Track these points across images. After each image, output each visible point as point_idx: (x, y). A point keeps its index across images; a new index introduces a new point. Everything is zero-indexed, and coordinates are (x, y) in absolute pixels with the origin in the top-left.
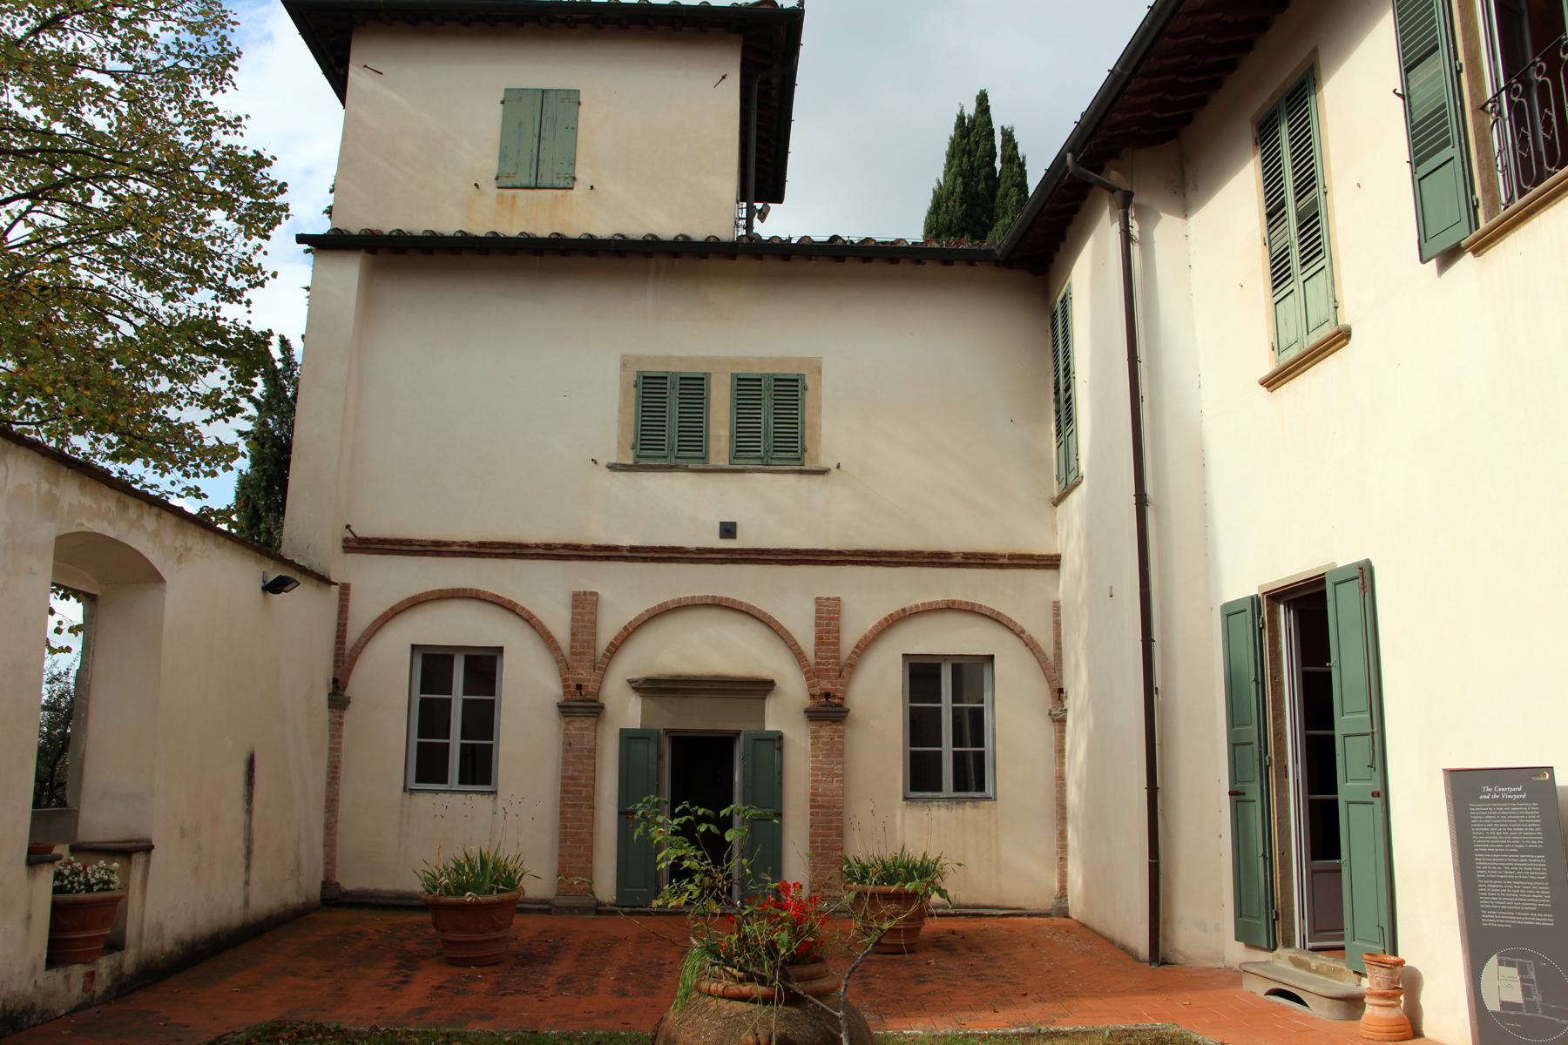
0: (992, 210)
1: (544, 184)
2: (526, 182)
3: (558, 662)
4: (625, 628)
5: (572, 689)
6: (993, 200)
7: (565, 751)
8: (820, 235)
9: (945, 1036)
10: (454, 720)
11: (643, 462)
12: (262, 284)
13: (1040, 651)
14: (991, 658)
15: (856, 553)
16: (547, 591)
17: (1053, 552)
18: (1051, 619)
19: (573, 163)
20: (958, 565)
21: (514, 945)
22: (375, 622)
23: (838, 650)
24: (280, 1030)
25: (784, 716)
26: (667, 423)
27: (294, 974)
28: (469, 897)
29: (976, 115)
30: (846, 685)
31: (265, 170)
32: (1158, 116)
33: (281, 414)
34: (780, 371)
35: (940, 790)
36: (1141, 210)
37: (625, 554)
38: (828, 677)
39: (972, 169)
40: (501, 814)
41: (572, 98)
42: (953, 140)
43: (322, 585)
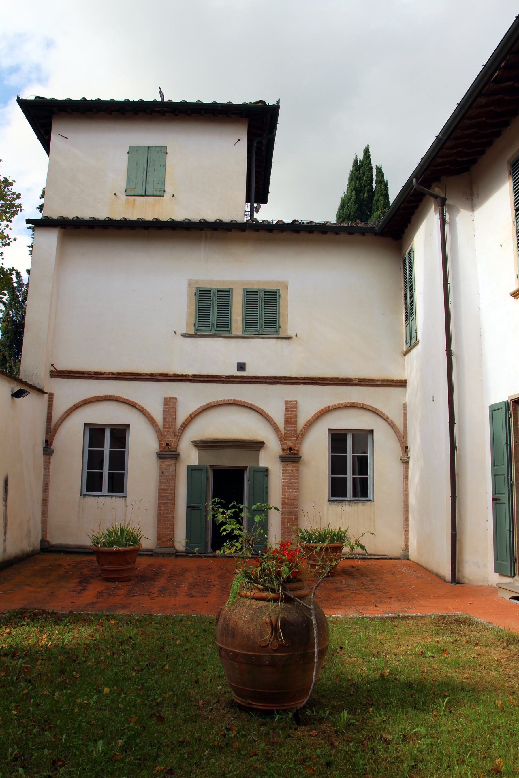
0: (371, 207)
1: (149, 194)
2: (140, 193)
3: (157, 432)
4: (190, 415)
5: (164, 446)
6: (372, 203)
7: (160, 476)
8: (288, 219)
9: (353, 618)
10: (106, 460)
11: (199, 333)
12: (9, 244)
13: (396, 428)
14: (372, 431)
15: (305, 378)
16: (151, 396)
17: (403, 379)
18: (402, 412)
19: (163, 183)
20: (356, 385)
21: (136, 572)
22: (66, 412)
24: (25, 612)
25: (269, 459)
26: (211, 312)
27: (30, 585)
28: (115, 548)
29: (363, 160)
30: (300, 444)
31: (10, 188)
32: (460, 160)
33: (16, 309)
35: (346, 496)
36: (450, 207)
38: (291, 440)
39: (361, 187)
40: (129, 508)
41: (163, 151)
42: (352, 172)
43: (40, 394)
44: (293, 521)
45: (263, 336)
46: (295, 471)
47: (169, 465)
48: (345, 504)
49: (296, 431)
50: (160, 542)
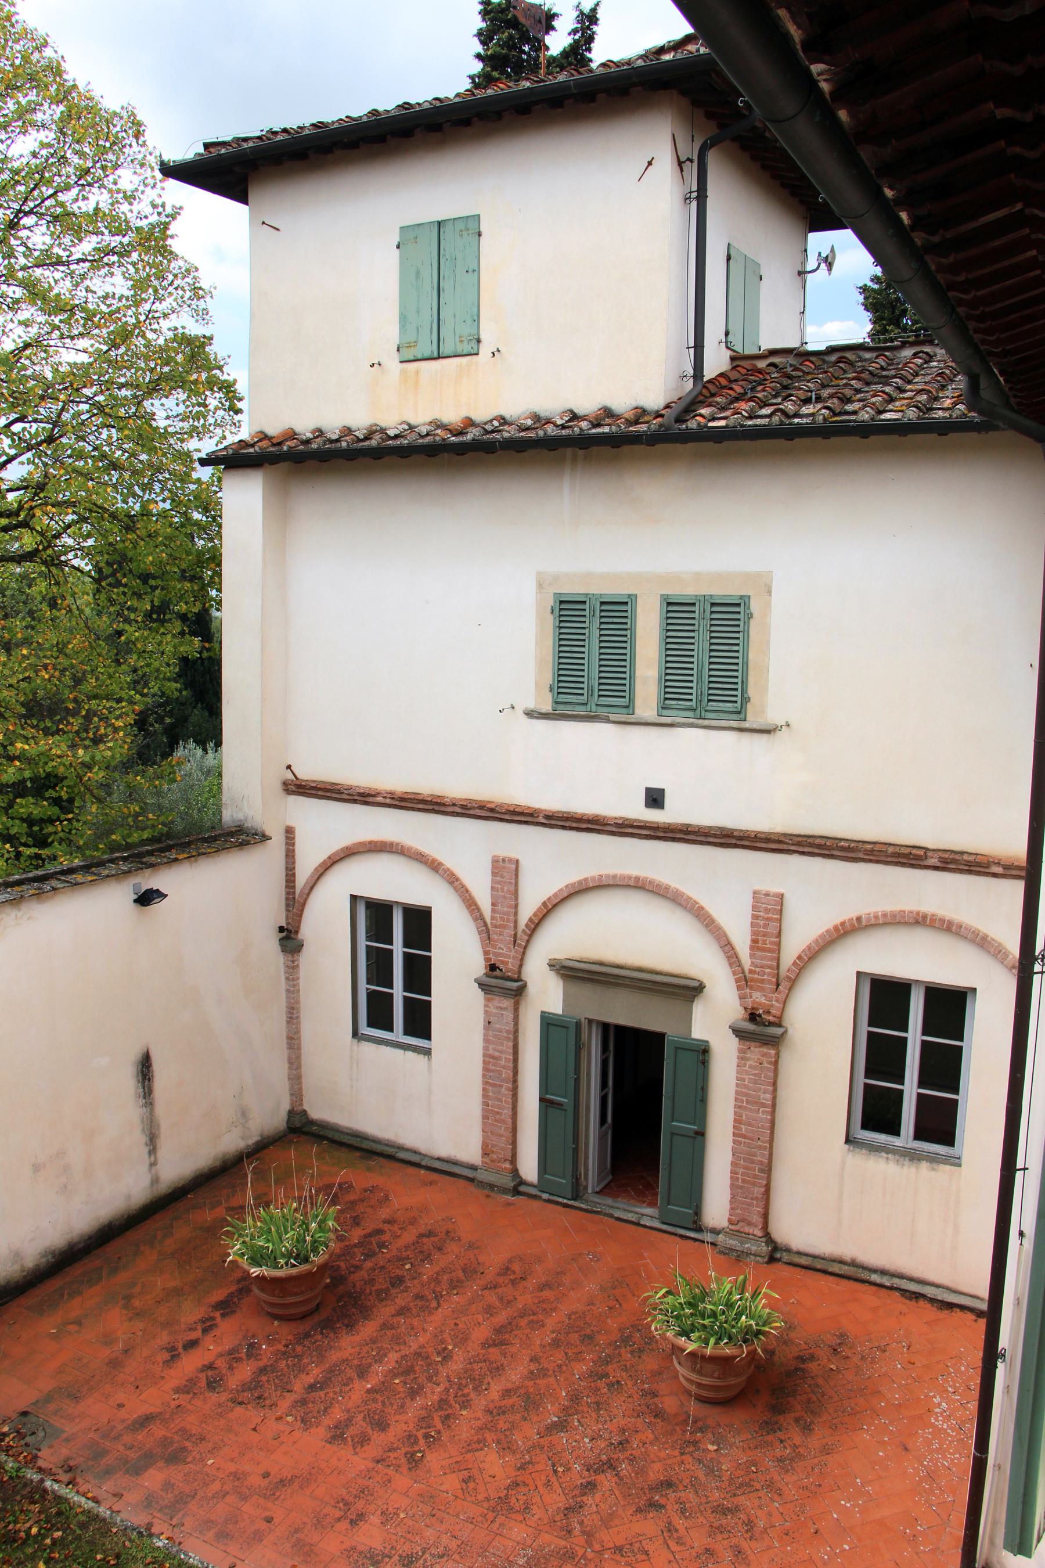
1: (447, 352)
2: (427, 354)
4: (544, 904)
19: (477, 320)
25: (714, 1021)
38: (762, 990)
45: (706, 722)
46: (766, 1065)
47: (501, 1008)
48: (887, 1159)
50: (487, 1160)
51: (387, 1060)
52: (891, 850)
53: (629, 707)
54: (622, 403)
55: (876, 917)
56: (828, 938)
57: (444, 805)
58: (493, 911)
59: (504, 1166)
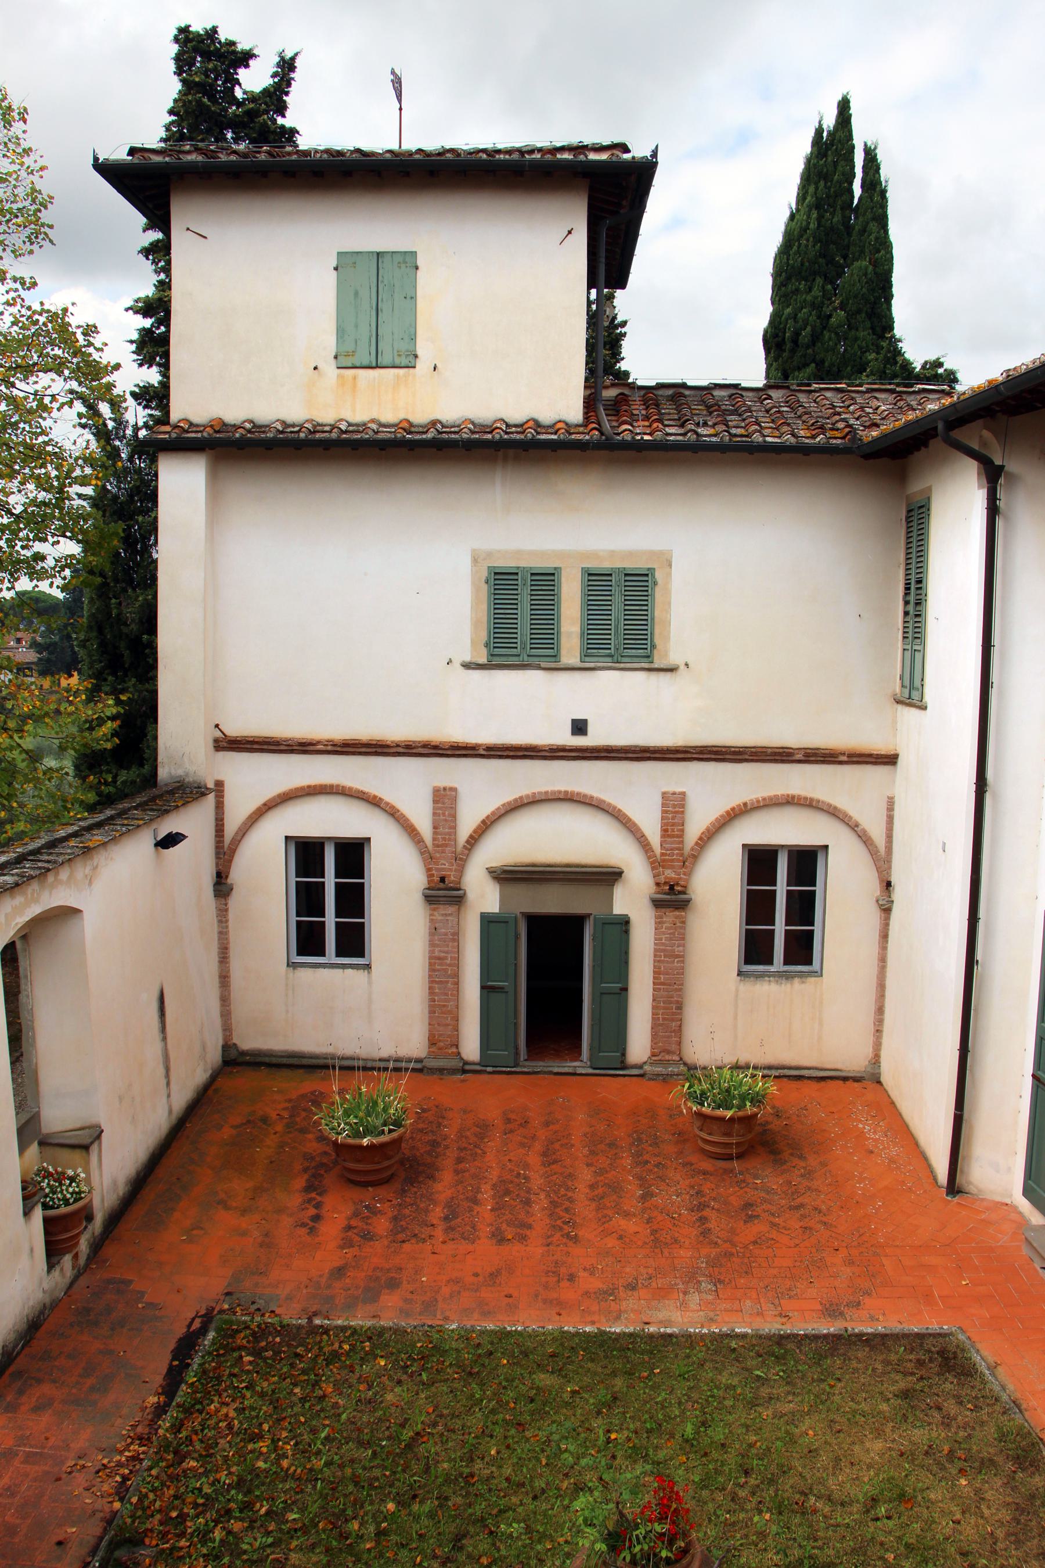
1: (384, 364)
2: (366, 363)
11: (496, 661)
16: (409, 785)
19: (413, 339)
23: (682, 842)
25: (632, 900)
30: (689, 874)
34: (630, 565)
37: (483, 752)
38: (672, 867)
41: (408, 261)
44: (673, 1014)
45: (622, 665)
47: (446, 915)
49: (681, 849)
51: (329, 980)
52: (769, 751)
53: (556, 657)
54: (547, 416)
55: (758, 801)
56: (722, 821)
57: (388, 746)
58: (435, 833)
59: (450, 1051)
